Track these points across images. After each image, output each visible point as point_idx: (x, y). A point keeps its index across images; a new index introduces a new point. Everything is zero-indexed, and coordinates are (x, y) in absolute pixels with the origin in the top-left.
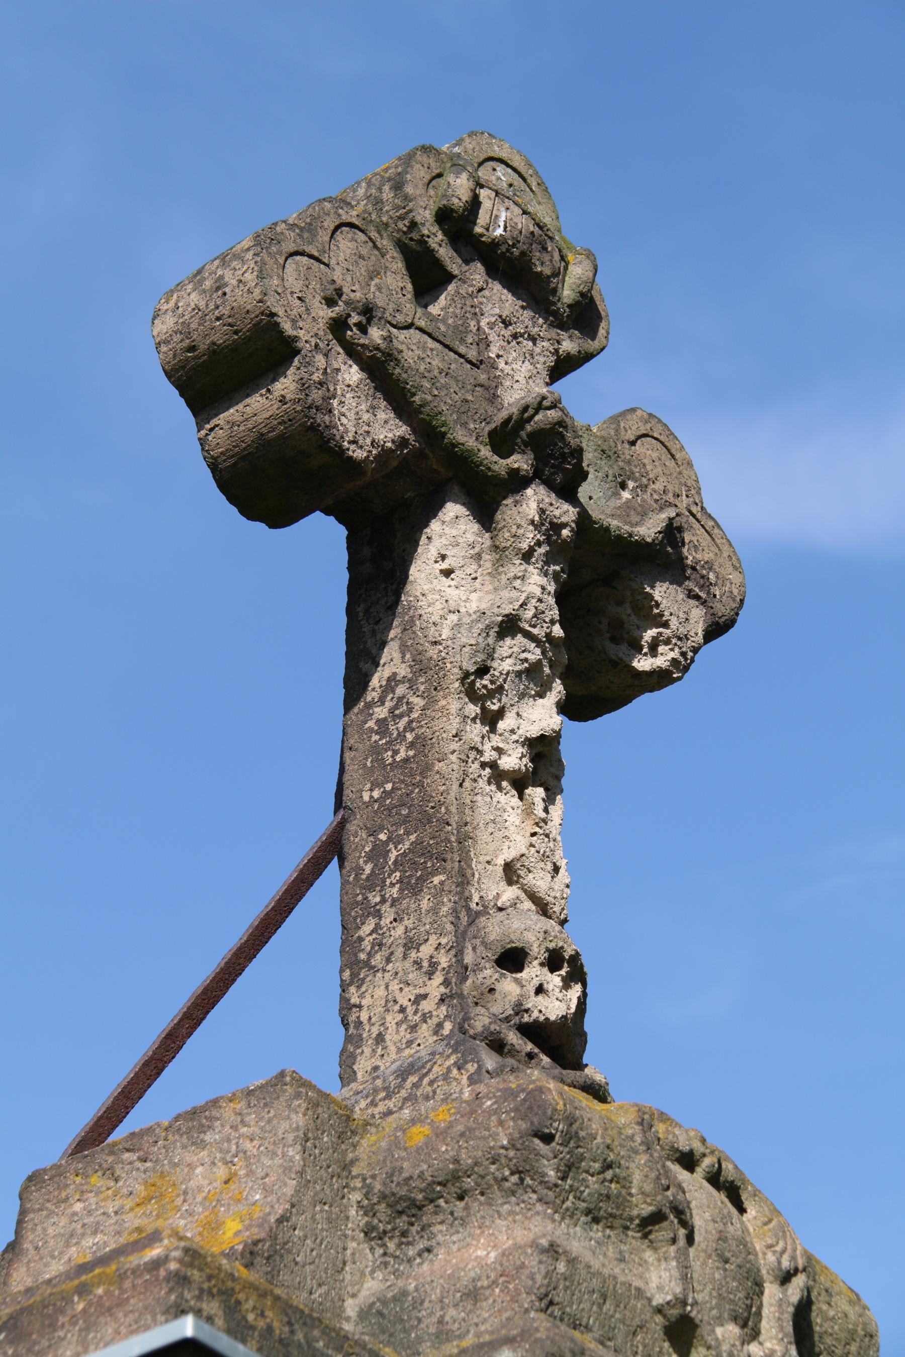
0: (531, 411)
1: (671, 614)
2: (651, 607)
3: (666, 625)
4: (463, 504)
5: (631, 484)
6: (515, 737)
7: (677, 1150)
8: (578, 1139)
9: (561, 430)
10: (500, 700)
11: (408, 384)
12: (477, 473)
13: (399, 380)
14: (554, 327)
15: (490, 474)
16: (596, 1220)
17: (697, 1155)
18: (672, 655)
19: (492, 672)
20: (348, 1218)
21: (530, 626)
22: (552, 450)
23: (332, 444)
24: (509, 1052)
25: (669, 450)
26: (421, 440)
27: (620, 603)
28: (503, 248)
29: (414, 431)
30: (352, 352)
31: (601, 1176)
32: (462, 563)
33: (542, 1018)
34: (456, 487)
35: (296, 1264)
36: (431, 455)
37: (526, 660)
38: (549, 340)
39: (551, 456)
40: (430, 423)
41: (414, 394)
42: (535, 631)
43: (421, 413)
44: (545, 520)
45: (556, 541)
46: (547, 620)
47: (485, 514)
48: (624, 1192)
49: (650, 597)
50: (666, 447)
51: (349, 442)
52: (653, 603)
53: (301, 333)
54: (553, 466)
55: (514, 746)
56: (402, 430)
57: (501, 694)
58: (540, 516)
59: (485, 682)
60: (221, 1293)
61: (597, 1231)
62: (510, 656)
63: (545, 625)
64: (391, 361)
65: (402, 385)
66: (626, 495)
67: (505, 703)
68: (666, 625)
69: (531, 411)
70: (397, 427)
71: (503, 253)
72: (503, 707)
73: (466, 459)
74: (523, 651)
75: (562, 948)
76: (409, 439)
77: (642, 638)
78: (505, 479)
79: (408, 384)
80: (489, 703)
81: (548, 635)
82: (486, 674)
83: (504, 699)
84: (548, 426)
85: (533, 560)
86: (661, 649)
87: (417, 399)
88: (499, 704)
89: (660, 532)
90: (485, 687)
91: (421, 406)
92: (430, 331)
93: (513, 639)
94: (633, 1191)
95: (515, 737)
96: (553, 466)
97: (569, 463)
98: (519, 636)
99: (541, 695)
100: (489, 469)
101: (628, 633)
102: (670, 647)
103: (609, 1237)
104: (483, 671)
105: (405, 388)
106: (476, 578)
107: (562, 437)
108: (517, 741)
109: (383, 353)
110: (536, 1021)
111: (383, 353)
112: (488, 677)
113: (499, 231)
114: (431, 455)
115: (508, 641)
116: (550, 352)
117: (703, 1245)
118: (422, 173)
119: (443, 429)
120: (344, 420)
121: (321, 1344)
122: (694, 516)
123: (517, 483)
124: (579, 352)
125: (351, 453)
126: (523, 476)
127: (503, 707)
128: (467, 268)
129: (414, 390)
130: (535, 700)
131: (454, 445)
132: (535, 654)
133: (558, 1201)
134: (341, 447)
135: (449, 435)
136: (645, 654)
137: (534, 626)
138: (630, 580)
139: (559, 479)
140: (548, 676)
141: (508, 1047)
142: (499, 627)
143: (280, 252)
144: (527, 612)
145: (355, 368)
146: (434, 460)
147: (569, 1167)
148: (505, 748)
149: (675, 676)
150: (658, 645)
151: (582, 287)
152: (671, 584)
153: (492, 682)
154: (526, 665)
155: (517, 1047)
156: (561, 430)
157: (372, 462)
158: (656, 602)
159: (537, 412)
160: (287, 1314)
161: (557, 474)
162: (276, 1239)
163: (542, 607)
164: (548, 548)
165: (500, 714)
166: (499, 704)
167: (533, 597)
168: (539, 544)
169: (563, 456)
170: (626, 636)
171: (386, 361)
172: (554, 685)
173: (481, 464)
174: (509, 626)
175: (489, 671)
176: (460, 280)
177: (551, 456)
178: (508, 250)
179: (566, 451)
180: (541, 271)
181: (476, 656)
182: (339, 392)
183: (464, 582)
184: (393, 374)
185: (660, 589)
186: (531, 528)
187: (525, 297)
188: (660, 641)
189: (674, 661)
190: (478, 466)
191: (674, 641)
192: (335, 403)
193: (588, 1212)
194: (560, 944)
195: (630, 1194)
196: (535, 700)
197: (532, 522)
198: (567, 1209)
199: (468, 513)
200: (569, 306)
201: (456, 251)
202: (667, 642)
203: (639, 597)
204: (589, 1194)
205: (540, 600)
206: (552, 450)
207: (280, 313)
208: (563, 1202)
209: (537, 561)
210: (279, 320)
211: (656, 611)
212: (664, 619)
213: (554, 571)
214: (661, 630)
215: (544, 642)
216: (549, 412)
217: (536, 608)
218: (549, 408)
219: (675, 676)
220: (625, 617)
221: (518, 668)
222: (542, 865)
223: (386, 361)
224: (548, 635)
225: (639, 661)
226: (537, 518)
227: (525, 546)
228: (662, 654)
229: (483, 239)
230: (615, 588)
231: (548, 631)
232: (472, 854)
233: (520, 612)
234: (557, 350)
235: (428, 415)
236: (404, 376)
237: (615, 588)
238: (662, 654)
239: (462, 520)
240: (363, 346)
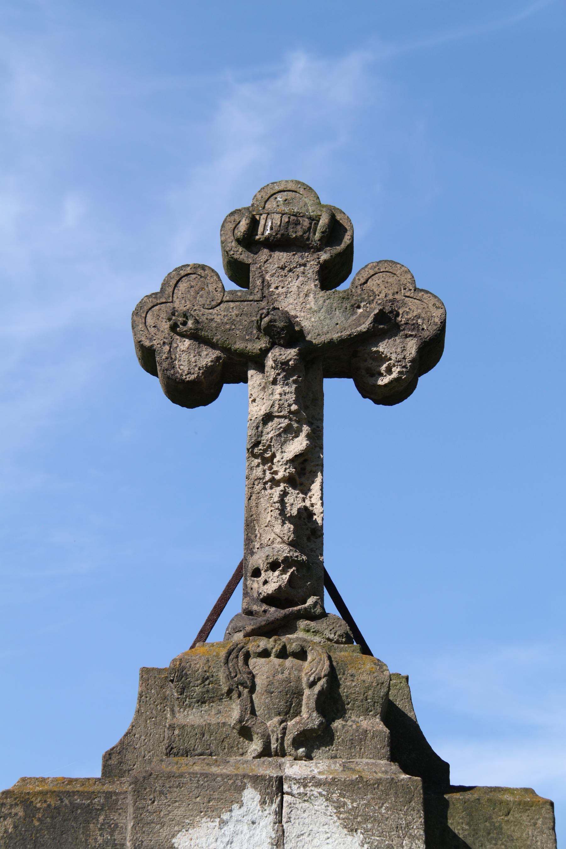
1: (391, 353)
2: (381, 355)
3: (390, 359)
4: (253, 369)
6: (280, 463)
7: (256, 653)
8: (187, 675)
10: (271, 451)
12: (250, 356)
16: (204, 702)
17: (269, 650)
18: (398, 370)
19: (262, 442)
20: (166, 718)
23: (177, 380)
24: (256, 613)
25: (392, 273)
28: (272, 238)
29: (222, 351)
30: (183, 335)
31: (203, 685)
32: (257, 394)
33: (265, 595)
35: (135, 749)
37: (281, 427)
39: (274, 335)
40: (223, 346)
41: (213, 339)
42: (281, 414)
45: (288, 368)
47: (261, 368)
48: (216, 686)
49: (378, 352)
51: (186, 375)
53: (155, 342)
54: (277, 338)
56: (217, 353)
57: (271, 448)
60: (21, 802)
61: (206, 707)
66: (360, 311)
68: (390, 359)
70: (213, 354)
71: (273, 240)
72: (274, 453)
75: (277, 559)
81: (290, 412)
87: (214, 340)
89: (371, 323)
90: (260, 450)
94: (221, 684)
95: (280, 463)
96: (277, 338)
97: (283, 334)
99: (297, 436)
100: (252, 353)
103: (212, 706)
104: (257, 444)
107: (275, 326)
108: (282, 465)
109: (194, 330)
110: (264, 597)
111: (194, 330)
112: (261, 445)
113: (268, 232)
115: (270, 424)
117: (260, 691)
118: (231, 226)
120: (182, 367)
121: (79, 800)
122: (408, 297)
124: (331, 256)
125: (188, 379)
126: (264, 350)
127: (274, 453)
131: (236, 351)
133: (181, 704)
134: (182, 379)
136: (385, 376)
137: (281, 412)
140: (297, 427)
141: (254, 612)
143: (143, 312)
145: (187, 340)
147: (183, 689)
152: (389, 339)
153: (263, 446)
154: (282, 429)
155: (258, 610)
159: (261, 321)
160: (59, 796)
162: (123, 743)
163: (281, 402)
164: (285, 373)
169: (279, 333)
172: (303, 428)
173: (249, 352)
174: (268, 418)
178: (274, 238)
179: (279, 330)
180: (296, 236)
182: (178, 356)
186: (273, 370)
189: (399, 372)
191: (396, 364)
192: (176, 362)
193: (198, 701)
194: (275, 558)
195: (220, 685)
197: (272, 367)
198: (186, 705)
200: (319, 240)
201: (250, 252)
202: (394, 366)
204: (196, 695)
205: (280, 400)
207: (143, 339)
208: (184, 703)
210: (143, 342)
211: (383, 356)
213: (293, 380)
214: (389, 362)
215: (289, 416)
218: (265, 317)
220: (370, 366)
221: (278, 432)
222: (276, 522)
224: (290, 412)
226: (274, 365)
227: (271, 379)
232: (256, 527)
233: (272, 410)
234: (319, 262)
240: (185, 331)
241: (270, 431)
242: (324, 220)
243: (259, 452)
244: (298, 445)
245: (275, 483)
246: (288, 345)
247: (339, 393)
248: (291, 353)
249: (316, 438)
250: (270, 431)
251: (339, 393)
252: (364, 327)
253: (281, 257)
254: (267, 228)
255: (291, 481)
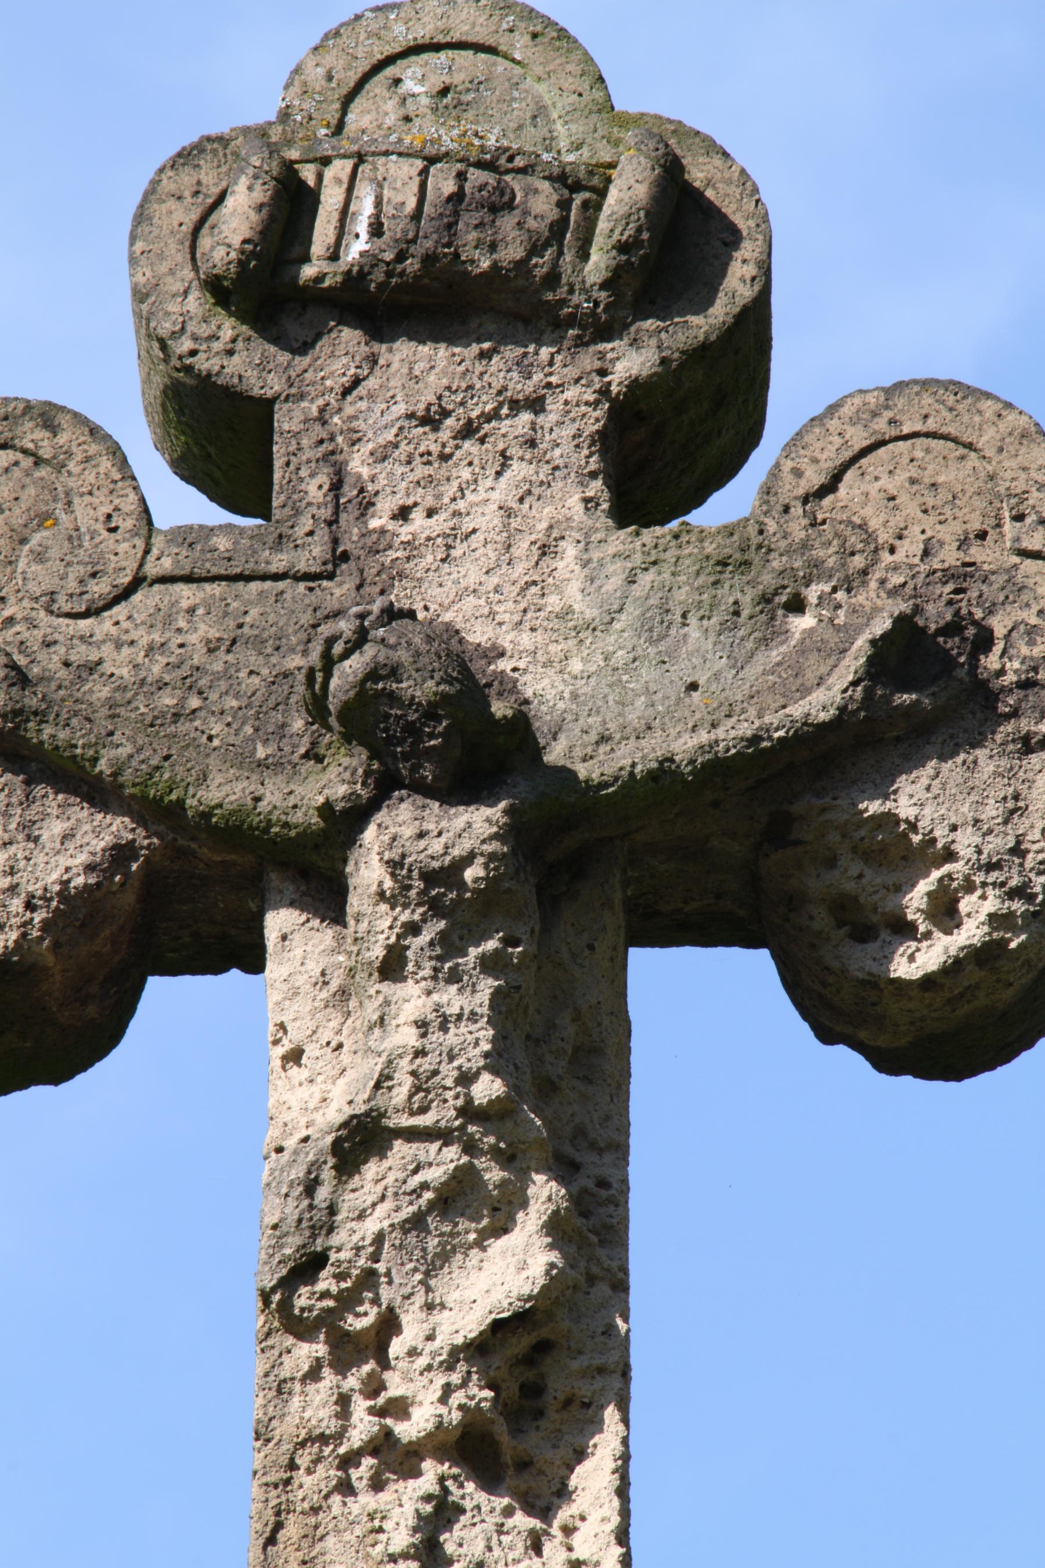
0: (319, 677)
2: (905, 835)
3: (950, 855)
4: (292, 904)
5: (812, 593)
6: (422, 1362)
9: (380, 686)
10: (376, 1301)
11: (75, 746)
13: (57, 748)
14: (587, 344)
15: (293, 833)
19: (333, 1257)
21: (412, 1114)
22: (386, 730)
25: (955, 440)
26: (162, 828)
27: (831, 863)
28: (378, 275)
29: (140, 820)
32: (312, 1025)
34: (273, 876)
36: (194, 846)
37: (424, 1186)
38: (577, 381)
40: (144, 797)
41: (95, 760)
43: (122, 786)
44: (410, 877)
45: (459, 901)
46: (449, 1082)
49: (890, 819)
50: (946, 437)
52: (903, 826)
55: (424, 1380)
56: (117, 828)
57: (375, 1287)
58: (393, 875)
59: (321, 1286)
62: (383, 1198)
63: (449, 1095)
64: (28, 720)
65: (67, 754)
67: (391, 1300)
69: (319, 677)
71: (381, 286)
72: (391, 1309)
73: (239, 827)
74: (415, 1172)
76: (134, 840)
77: (902, 909)
78: (323, 830)
79: (75, 746)
80: (350, 1319)
81: (468, 1112)
82: (323, 1267)
83: (386, 1294)
84: (352, 694)
85: (410, 967)
86: (965, 905)
88: (375, 1310)
89: (855, 683)
91: (115, 774)
92: (186, 571)
93: (383, 1156)
95: (422, 1362)
97: (432, 736)
98: (398, 1144)
99: (502, 1229)
100: (286, 825)
101: (875, 910)
102: (979, 892)
104: (308, 1266)
105: (75, 756)
106: (340, 1046)
108: (429, 1368)
114: (194, 846)
116: (587, 403)
118: (179, 216)
119: (173, 797)
123: (345, 823)
126: (345, 812)
127: (391, 1309)
128: (308, 359)
129: (91, 752)
130: (484, 1249)
131: (206, 815)
132: (443, 1162)
135: (188, 802)
137: (423, 1110)
138: (824, 810)
139: (428, 773)
140: (503, 1184)
142: (334, 1155)
144: (395, 1091)
146: (205, 850)
148: (409, 1394)
149: (1013, 945)
150: (957, 901)
151: (617, 232)
152: (943, 758)
153: (340, 1277)
156: (380, 686)
157: (41, 939)
158: (907, 821)
161: (421, 766)
164: (442, 924)
165: (389, 1324)
166: (375, 1310)
167: (400, 1056)
168: (413, 929)
169: (413, 730)
170: (875, 919)
171: (17, 727)
172: (531, 1191)
173: (269, 824)
174: (361, 1140)
175: (327, 1258)
176: (286, 400)
177: (390, 741)
178: (389, 274)
179: (413, 717)
181: (282, 1247)
183: (321, 1063)
184: (42, 743)
185: (909, 789)
187: (491, 327)
188: (956, 890)
190: (266, 831)
191: (978, 879)
196: (484, 1249)
199: (304, 917)
200: (604, 286)
202: (969, 887)
203: (862, 833)
205: (419, 1053)
206: (386, 730)
209: (418, 966)
211: (916, 839)
212: (940, 845)
214: (947, 868)
215: (462, 1128)
216: (347, 663)
217: (414, 1073)
218: (346, 655)
219: (1013, 945)
220: (850, 887)
223: (17, 727)
224: (468, 1112)
225: (912, 958)
227: (378, 952)
228: (969, 915)
229: (326, 284)
230: (798, 843)
231: (460, 1102)
234: (604, 392)
235: (134, 785)
236: (63, 735)
237: (798, 843)
238: (969, 915)
239: (297, 936)
241: (374, 1202)
242: (629, 190)
243: (324, 1308)
244: (507, 1270)
245: (394, 1458)
246: (459, 789)
247: (701, 1013)
248: (471, 829)
249: (594, 1235)
250: (374, 1202)
251: (701, 1013)
252: (821, 702)
253: (424, 367)
254: (346, 237)
255: (472, 1448)
